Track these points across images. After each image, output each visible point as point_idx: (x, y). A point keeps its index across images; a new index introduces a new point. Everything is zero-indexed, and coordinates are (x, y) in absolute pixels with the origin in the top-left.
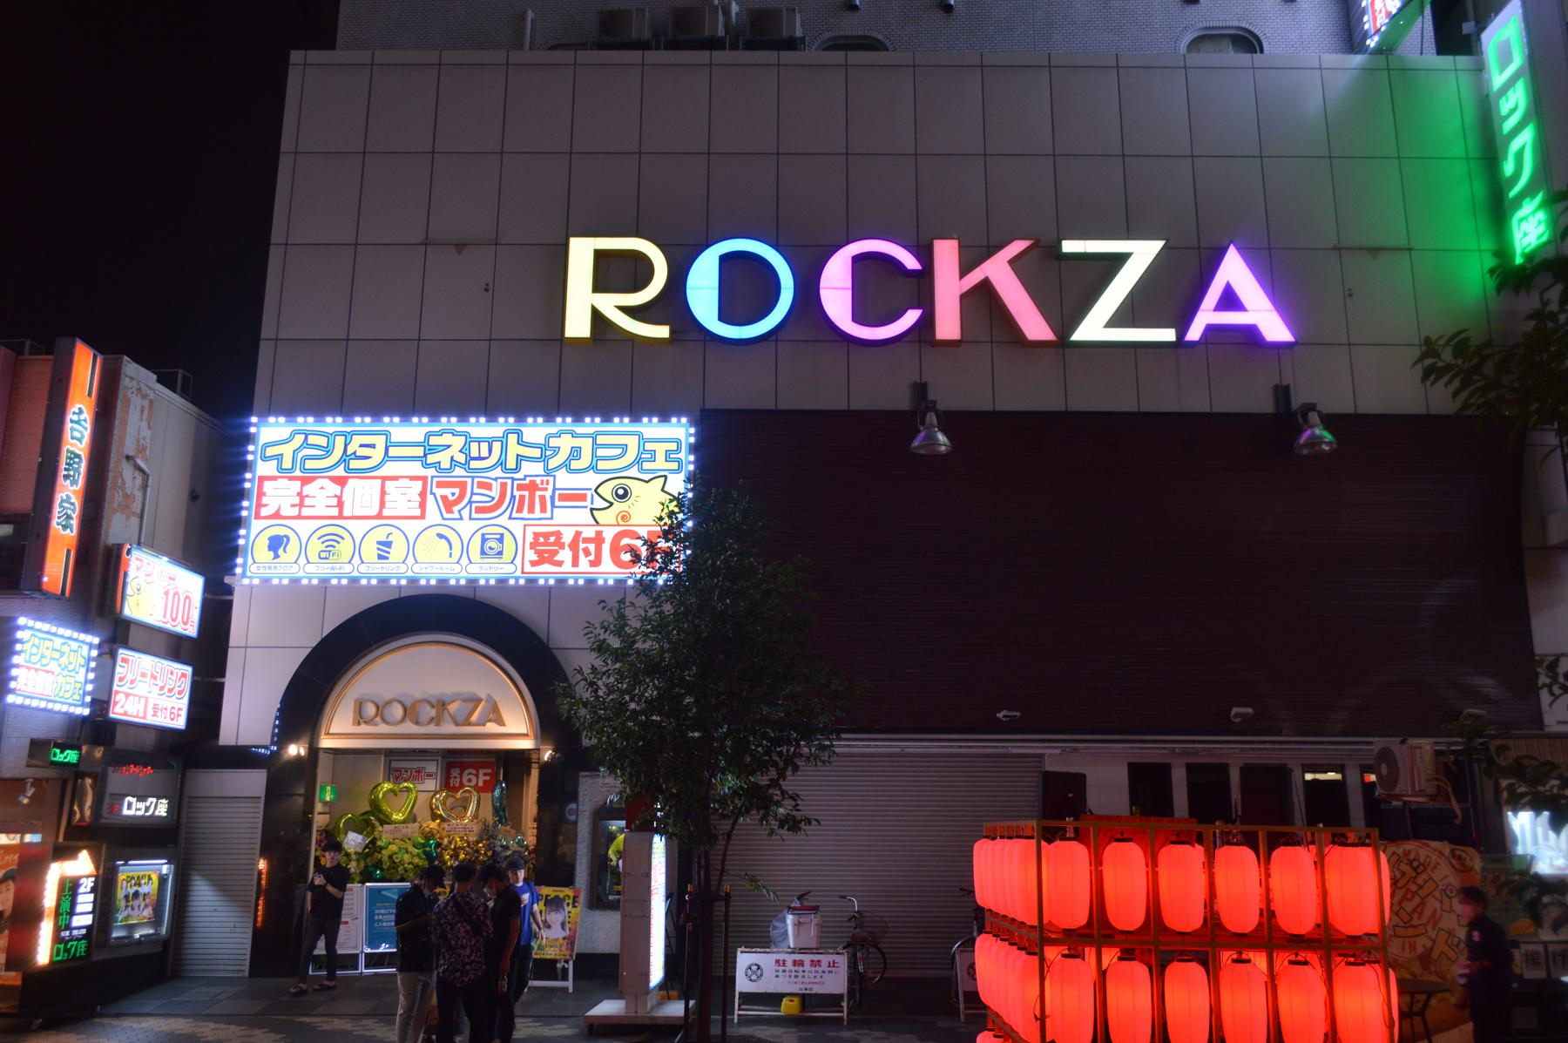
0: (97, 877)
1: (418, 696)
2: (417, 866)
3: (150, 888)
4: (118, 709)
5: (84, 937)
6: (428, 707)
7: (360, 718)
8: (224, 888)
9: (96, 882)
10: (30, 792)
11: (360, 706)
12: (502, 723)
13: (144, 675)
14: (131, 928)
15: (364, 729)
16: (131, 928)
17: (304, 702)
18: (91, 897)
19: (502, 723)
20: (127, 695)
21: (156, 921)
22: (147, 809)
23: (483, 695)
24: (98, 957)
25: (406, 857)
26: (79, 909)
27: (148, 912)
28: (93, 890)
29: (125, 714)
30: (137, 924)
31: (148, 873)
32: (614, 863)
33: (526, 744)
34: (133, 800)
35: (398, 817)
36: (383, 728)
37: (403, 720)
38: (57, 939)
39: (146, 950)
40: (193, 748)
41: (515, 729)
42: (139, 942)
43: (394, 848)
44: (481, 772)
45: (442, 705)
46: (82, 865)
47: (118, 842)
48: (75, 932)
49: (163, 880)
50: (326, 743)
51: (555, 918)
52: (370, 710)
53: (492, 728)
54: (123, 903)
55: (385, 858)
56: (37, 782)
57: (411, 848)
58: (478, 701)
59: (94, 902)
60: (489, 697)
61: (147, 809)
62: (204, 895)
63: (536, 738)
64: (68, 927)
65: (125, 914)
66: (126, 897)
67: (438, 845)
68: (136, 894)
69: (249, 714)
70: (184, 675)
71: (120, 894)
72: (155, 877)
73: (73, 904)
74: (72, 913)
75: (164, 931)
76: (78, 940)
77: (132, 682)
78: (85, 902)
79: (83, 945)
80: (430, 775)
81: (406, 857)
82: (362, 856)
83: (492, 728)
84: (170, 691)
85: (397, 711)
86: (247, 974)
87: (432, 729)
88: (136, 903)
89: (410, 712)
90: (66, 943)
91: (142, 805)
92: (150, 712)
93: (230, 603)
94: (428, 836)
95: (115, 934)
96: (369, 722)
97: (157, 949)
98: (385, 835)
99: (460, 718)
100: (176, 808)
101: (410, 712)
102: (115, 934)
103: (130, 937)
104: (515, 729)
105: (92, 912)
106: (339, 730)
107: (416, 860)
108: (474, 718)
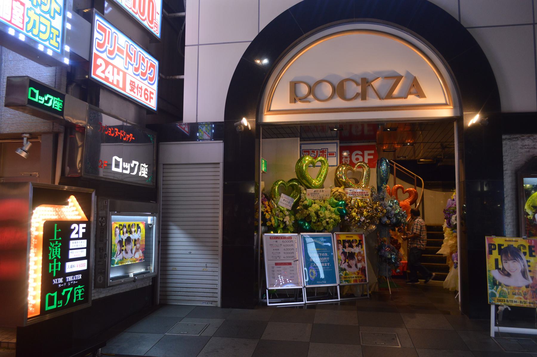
0: (88, 223)
1: (345, 76)
2: (335, 220)
3: (139, 235)
4: (99, 72)
5: (79, 282)
6: (354, 85)
7: (295, 97)
8: (196, 236)
9: (88, 229)
10: (27, 146)
11: (294, 85)
12: (420, 94)
13: (119, 50)
14: (126, 268)
15: (299, 105)
16: (126, 268)
17: (247, 87)
18: (84, 243)
19: (420, 94)
20: (107, 64)
21: (146, 262)
22: (132, 169)
23: (402, 73)
24: (96, 295)
25: (327, 213)
26: (72, 255)
27: (139, 255)
28: (86, 236)
29: (107, 79)
30: (129, 264)
31: (132, 226)
32: (530, 217)
33: (446, 112)
34: (120, 160)
35: (316, 182)
36: (316, 104)
37: (332, 97)
38: (48, 285)
39: (140, 285)
40: (162, 125)
41: (435, 101)
42: (134, 280)
43: (316, 206)
44: (366, 153)
45: (365, 83)
46: (72, 210)
47: (107, 196)
48: (70, 278)
49: (148, 228)
50: (268, 118)
51: (515, 267)
52: (304, 90)
53: (412, 99)
54: (117, 248)
55: (313, 214)
56: (33, 136)
57: (329, 207)
58: (398, 78)
59: (88, 248)
60: (408, 74)
61: (132, 169)
62: (180, 241)
63: (455, 107)
64: (62, 273)
65: (120, 257)
66: (120, 242)
67: (346, 205)
68: (128, 240)
69: (204, 99)
70: (152, 66)
71: (115, 240)
72: (142, 226)
73: (65, 249)
74: (65, 258)
75: (152, 268)
76: (74, 286)
77: (111, 53)
78: (78, 248)
79: (79, 290)
80: (332, 154)
81: (327, 213)
82: (294, 210)
83: (412, 99)
84: (144, 74)
85: (327, 90)
86: (219, 305)
87: (358, 103)
88: (129, 247)
89: (339, 90)
90: (60, 290)
91: (127, 165)
92: (128, 87)
93: (183, 18)
94: (339, 197)
95: (112, 275)
96: (304, 99)
97: (149, 283)
98: (308, 196)
99: (384, 93)
100: (154, 172)
101: (339, 90)
102: (112, 275)
103: (126, 276)
104: (435, 101)
105: (87, 258)
106: (279, 108)
107: (334, 216)
108: (396, 92)
